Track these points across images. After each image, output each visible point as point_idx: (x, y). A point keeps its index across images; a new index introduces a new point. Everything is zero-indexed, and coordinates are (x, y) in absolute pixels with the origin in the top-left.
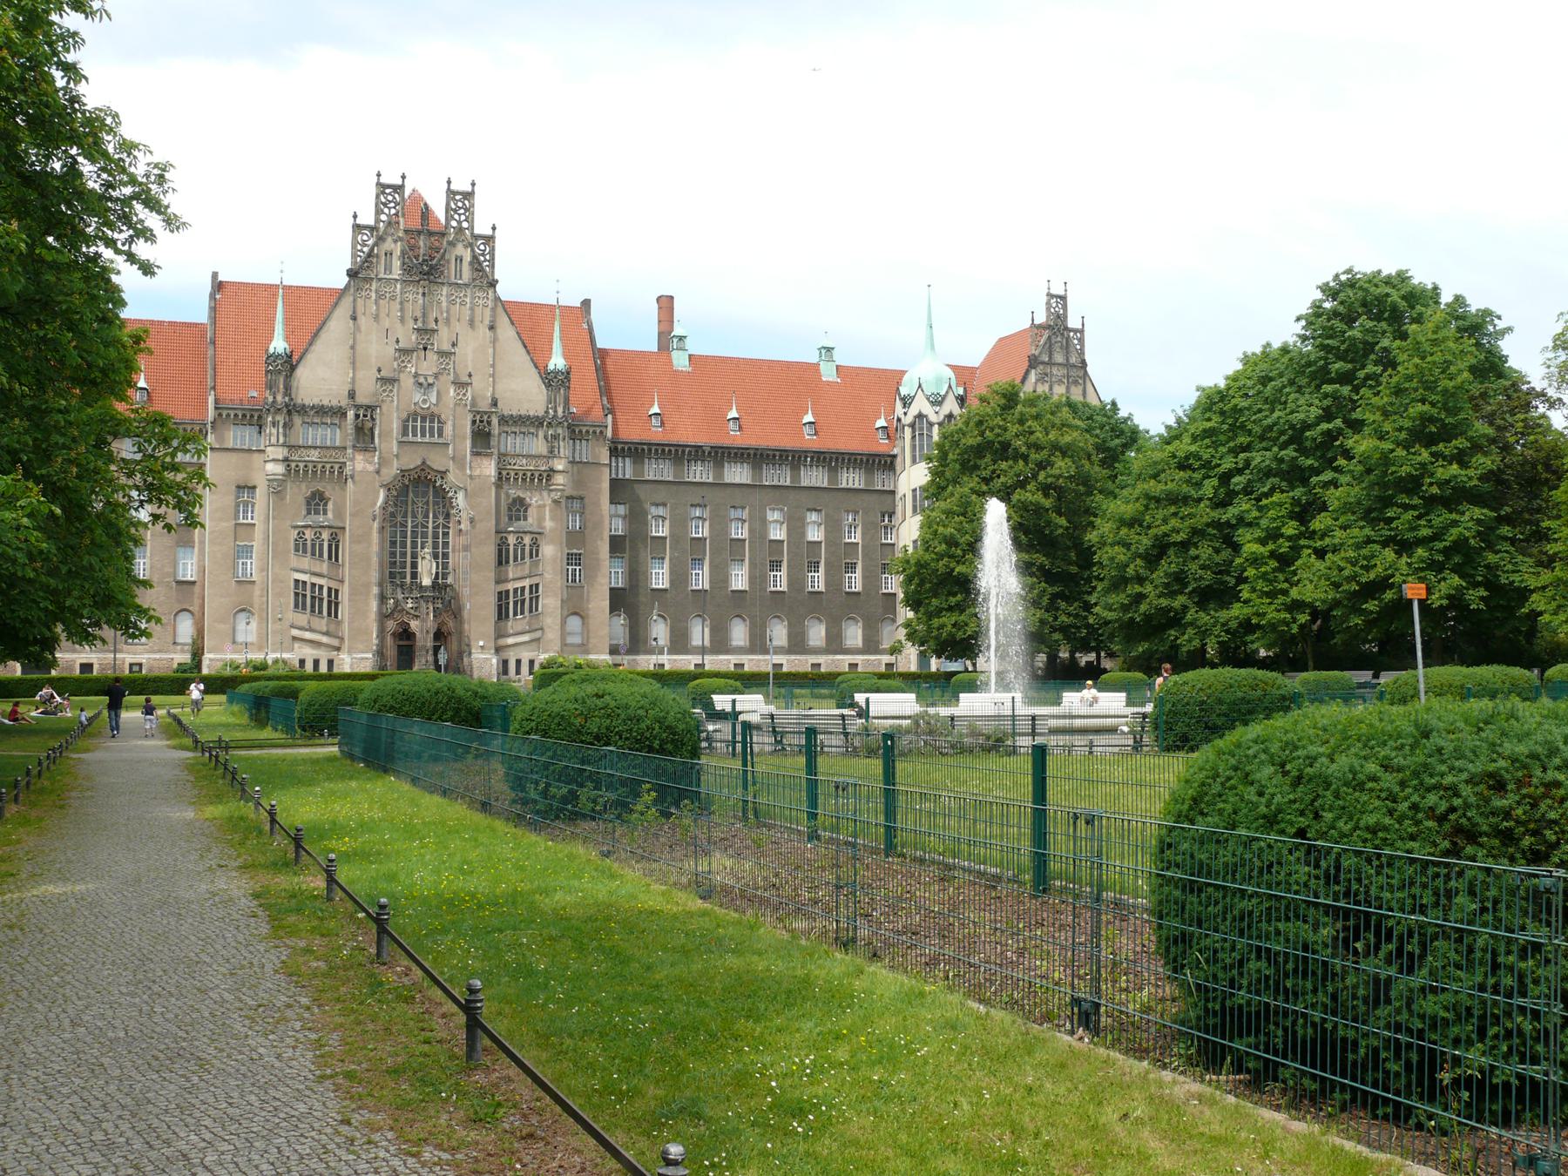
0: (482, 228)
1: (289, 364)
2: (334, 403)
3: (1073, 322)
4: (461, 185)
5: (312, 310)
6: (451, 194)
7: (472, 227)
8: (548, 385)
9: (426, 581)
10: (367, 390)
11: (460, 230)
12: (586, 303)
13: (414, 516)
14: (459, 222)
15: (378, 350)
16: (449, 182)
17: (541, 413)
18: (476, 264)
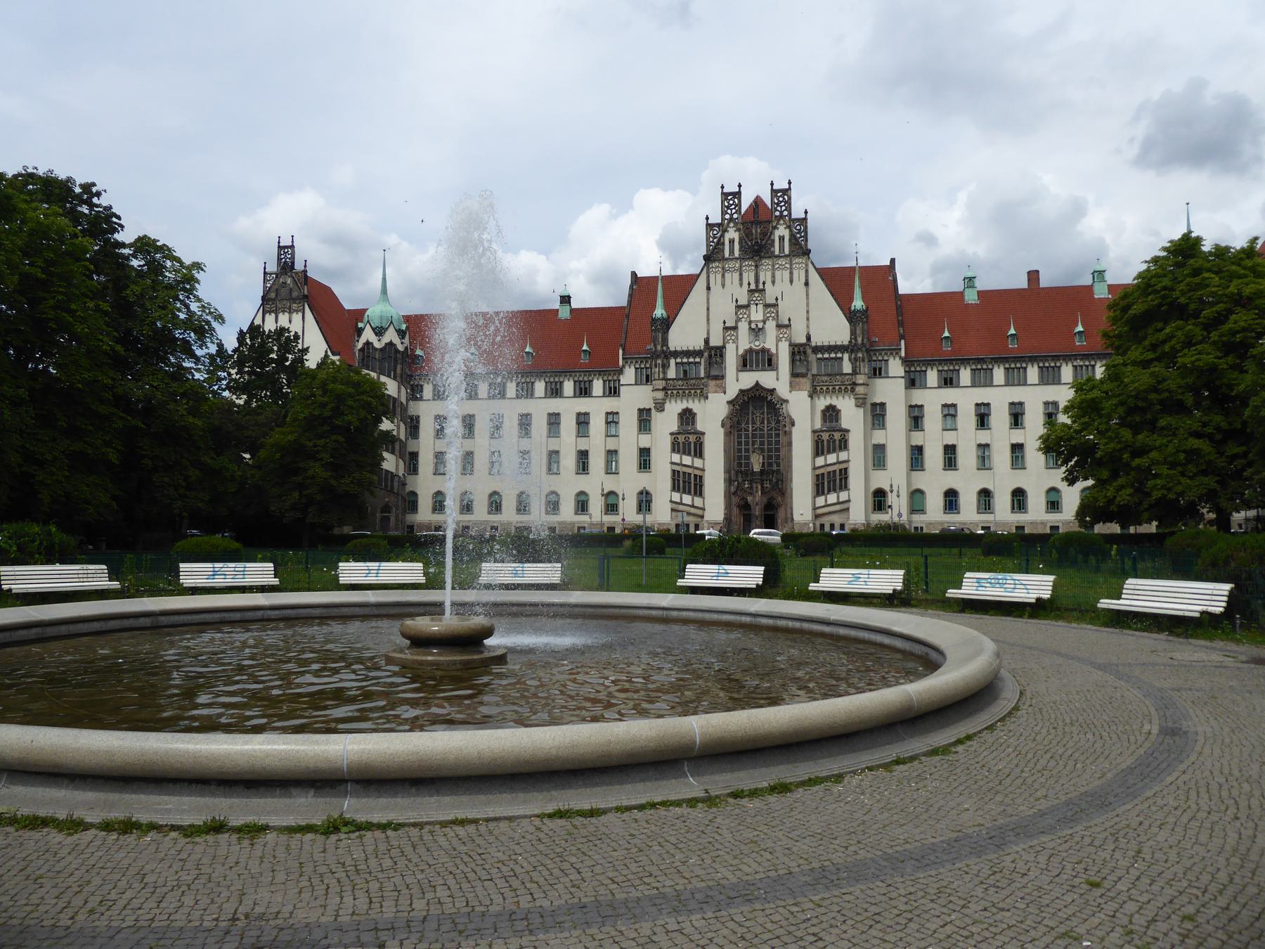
0: (797, 213)
1: (667, 323)
2: (697, 348)
4: (781, 184)
5: (678, 289)
9: (757, 468)
10: (716, 341)
11: (781, 216)
12: (893, 261)
13: (754, 423)
14: (781, 212)
15: (723, 310)
16: (772, 184)
17: (846, 343)
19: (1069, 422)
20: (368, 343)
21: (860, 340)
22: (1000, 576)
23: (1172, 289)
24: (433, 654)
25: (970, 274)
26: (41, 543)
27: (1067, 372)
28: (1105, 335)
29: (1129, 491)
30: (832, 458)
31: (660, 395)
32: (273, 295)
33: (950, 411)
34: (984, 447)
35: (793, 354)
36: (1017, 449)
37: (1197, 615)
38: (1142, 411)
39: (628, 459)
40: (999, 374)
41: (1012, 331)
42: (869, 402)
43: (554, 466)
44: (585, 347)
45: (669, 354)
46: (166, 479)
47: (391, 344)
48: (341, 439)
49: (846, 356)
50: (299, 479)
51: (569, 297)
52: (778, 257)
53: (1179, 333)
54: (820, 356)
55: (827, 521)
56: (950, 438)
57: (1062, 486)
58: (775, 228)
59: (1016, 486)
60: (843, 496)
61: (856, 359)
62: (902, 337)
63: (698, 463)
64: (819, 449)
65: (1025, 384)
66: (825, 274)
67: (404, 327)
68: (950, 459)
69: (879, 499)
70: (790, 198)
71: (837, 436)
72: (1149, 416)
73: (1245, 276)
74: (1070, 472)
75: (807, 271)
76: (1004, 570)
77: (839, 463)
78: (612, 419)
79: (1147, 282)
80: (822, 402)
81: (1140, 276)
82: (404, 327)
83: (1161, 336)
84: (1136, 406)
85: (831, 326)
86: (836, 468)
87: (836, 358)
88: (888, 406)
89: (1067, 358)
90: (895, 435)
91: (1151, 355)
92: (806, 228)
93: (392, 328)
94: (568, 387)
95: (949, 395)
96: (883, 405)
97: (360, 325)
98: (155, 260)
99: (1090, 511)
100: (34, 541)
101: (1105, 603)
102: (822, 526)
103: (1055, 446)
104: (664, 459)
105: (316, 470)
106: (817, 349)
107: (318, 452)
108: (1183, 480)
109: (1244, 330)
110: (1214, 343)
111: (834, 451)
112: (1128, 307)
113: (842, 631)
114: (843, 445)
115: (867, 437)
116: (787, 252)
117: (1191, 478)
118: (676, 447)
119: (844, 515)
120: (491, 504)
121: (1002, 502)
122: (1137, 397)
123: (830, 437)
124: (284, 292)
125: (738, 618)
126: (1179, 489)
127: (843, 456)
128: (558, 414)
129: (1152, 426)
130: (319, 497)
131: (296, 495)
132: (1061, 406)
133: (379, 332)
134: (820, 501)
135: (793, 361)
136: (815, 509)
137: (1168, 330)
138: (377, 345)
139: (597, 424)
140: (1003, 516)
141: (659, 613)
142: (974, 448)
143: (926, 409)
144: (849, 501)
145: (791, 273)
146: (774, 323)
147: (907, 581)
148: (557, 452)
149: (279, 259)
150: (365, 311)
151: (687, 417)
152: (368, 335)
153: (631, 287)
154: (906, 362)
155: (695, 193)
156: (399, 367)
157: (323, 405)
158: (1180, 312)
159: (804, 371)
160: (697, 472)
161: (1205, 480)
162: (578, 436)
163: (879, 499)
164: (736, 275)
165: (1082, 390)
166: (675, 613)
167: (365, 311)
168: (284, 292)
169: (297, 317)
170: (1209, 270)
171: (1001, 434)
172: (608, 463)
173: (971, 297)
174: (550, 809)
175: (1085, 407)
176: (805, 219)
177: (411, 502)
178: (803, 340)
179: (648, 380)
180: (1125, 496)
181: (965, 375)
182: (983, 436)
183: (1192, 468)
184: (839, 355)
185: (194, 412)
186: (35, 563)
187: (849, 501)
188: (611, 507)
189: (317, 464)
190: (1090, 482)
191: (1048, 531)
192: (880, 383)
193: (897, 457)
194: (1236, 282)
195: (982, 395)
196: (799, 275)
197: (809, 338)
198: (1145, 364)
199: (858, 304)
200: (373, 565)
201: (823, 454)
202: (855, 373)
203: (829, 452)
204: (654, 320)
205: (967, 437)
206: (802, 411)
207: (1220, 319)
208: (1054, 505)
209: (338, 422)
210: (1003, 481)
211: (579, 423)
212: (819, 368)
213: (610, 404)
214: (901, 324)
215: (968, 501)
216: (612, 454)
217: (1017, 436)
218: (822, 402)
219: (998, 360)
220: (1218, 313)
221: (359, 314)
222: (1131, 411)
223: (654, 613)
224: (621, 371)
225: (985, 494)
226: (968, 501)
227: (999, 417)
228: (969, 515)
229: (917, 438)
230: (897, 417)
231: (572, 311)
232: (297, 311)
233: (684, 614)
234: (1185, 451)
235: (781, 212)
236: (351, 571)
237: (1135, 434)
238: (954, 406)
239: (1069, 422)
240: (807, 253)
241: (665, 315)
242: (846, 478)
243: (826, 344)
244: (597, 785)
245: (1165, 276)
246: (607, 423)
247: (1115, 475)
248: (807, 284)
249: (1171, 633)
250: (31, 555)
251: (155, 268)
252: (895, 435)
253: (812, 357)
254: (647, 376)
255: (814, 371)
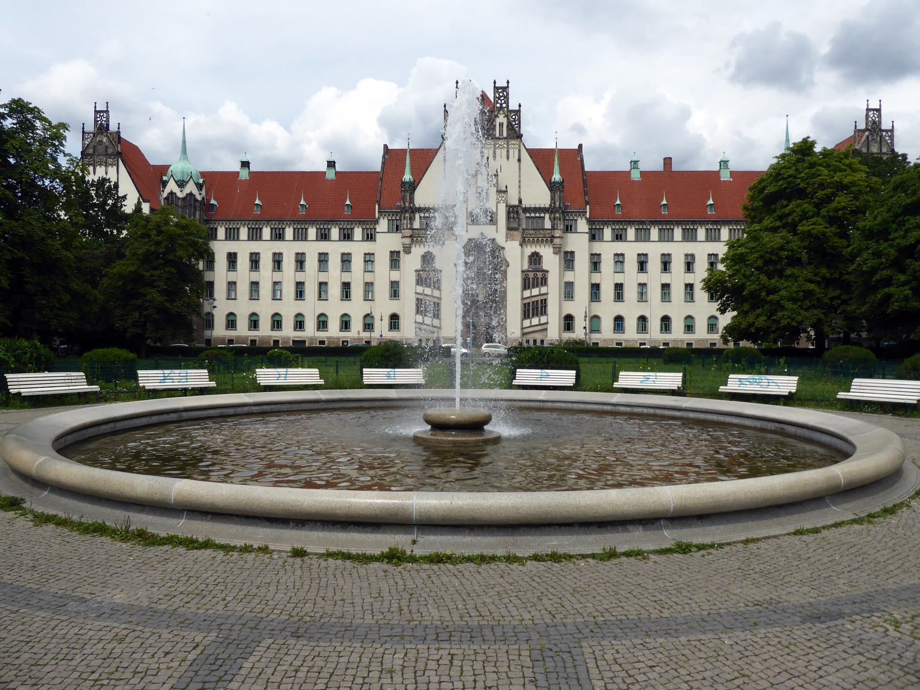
0: (513, 106)
3: (885, 125)
4: (501, 83)
6: (496, 89)
7: (508, 106)
8: (551, 190)
11: (501, 108)
12: (580, 146)
14: (501, 104)
16: (495, 82)
17: (547, 206)
18: (510, 127)
19: (724, 269)
20: (172, 193)
21: (557, 204)
22: (757, 377)
23: (795, 177)
24: (452, 436)
25: (635, 159)
26: (31, 355)
27: (725, 233)
28: (745, 208)
29: (765, 318)
30: (535, 291)
31: (408, 241)
32: (91, 151)
33: (619, 259)
34: (642, 285)
35: (508, 213)
36: (689, 287)
37: (915, 402)
38: (773, 264)
39: (382, 290)
40: (654, 233)
41: (664, 202)
42: (563, 250)
43: (323, 297)
44: (348, 202)
45: (415, 210)
46: (43, 302)
47: (191, 194)
48: (173, 270)
49: (547, 216)
50: (139, 302)
51: (334, 162)
52: (499, 139)
53: (798, 210)
54: (528, 215)
55: (531, 337)
56: (619, 279)
57: (718, 314)
58: (496, 116)
59: (664, 314)
60: (543, 319)
61: (554, 218)
62: (587, 203)
63: (436, 293)
64: (526, 285)
65: (672, 241)
66: (535, 154)
67: (201, 181)
68: (619, 294)
69: (568, 322)
70: (508, 94)
71: (540, 275)
72: (779, 267)
73: (845, 170)
74: (723, 304)
75: (520, 151)
76: (760, 373)
77: (540, 295)
78: (369, 259)
79: (776, 173)
80: (529, 250)
81: (772, 167)
82: (201, 181)
83: (787, 210)
84: (770, 259)
85: (537, 194)
86: (539, 298)
87: (540, 217)
88: (576, 254)
89: (702, 223)
90: (581, 275)
91: (778, 223)
92: (519, 118)
93: (191, 181)
94: (335, 233)
95: (619, 247)
96: (572, 253)
97: (165, 178)
98: (27, 119)
99: (732, 331)
100: (26, 353)
101: (842, 395)
102: (528, 341)
103: (715, 287)
104: (409, 289)
105: (154, 295)
106: (526, 210)
107: (154, 281)
108: (802, 312)
109: (844, 208)
110: (824, 217)
111: (537, 286)
112: (764, 188)
113: (691, 415)
114: (544, 282)
115: (561, 276)
116: (505, 135)
117: (807, 310)
118: (420, 281)
119: (544, 333)
120: (228, 321)
121: (654, 325)
122: (771, 253)
123: (535, 276)
124: (100, 149)
125: (601, 407)
126: (799, 318)
127: (544, 290)
128: (327, 254)
129: (781, 274)
130: (156, 317)
131: (137, 314)
132: (720, 256)
133: (181, 184)
134: (527, 323)
135: (508, 218)
136: (522, 328)
137: (790, 207)
138: (180, 195)
139: (357, 262)
140: (655, 336)
141: (537, 404)
142: (636, 285)
143: (603, 257)
144: (547, 323)
145: (508, 151)
146: (495, 189)
147: (684, 381)
148: (326, 283)
149: (96, 121)
150: (170, 166)
151: (427, 258)
152: (172, 186)
153: (384, 157)
154: (590, 222)
155: (402, 84)
156: (198, 213)
157: (158, 243)
158: (800, 193)
159: (516, 226)
160: (436, 300)
161: (816, 312)
162: (342, 271)
163: (568, 322)
164: (504, 152)
165: (733, 247)
166: (549, 405)
167: (170, 166)
168: (100, 149)
169: (112, 171)
170: (820, 165)
171: (654, 276)
172: (366, 292)
173: (636, 176)
174: (792, 529)
175: (735, 258)
176: (519, 111)
177: (209, 322)
178: (516, 203)
179: (397, 229)
180: (761, 321)
181: (631, 233)
182: (643, 278)
183: (807, 303)
184: (542, 215)
185: (66, 246)
186: (29, 372)
187: (547, 323)
188: (368, 326)
189: (154, 290)
190: (735, 313)
191: (685, 346)
192: (571, 236)
193: (582, 292)
194: (839, 174)
195: (643, 247)
196: (514, 154)
197: (520, 201)
198: (774, 230)
199: (557, 177)
200: (282, 371)
201: (529, 288)
202: (553, 228)
203: (533, 287)
204: (404, 183)
205: (631, 277)
206: (515, 255)
207: (829, 199)
208: (712, 327)
209: (171, 257)
210: (677, 310)
211: (343, 261)
212: (527, 224)
213: (368, 247)
214: (586, 193)
215: (631, 324)
216: (323, 285)
217: (690, 278)
218: (529, 250)
219: (654, 223)
220: (826, 195)
221: (164, 169)
222: (768, 262)
223: (532, 404)
224: (376, 222)
225: (643, 319)
226: (631, 324)
227: (654, 264)
228: (631, 335)
229: (596, 278)
230: (582, 262)
231: (336, 173)
232: (112, 165)
233: (557, 404)
234: (803, 291)
235: (501, 104)
236: (149, 378)
237: (770, 279)
238: (623, 255)
239: (724, 269)
240: (520, 136)
241: (412, 180)
242: (546, 306)
243: (533, 206)
244: (792, 514)
245: (790, 168)
246: (365, 261)
247: (754, 307)
248: (519, 160)
249: (894, 414)
250: (25, 364)
251: (26, 126)
252: (581, 275)
253: (522, 216)
254: (397, 226)
255: (524, 226)
